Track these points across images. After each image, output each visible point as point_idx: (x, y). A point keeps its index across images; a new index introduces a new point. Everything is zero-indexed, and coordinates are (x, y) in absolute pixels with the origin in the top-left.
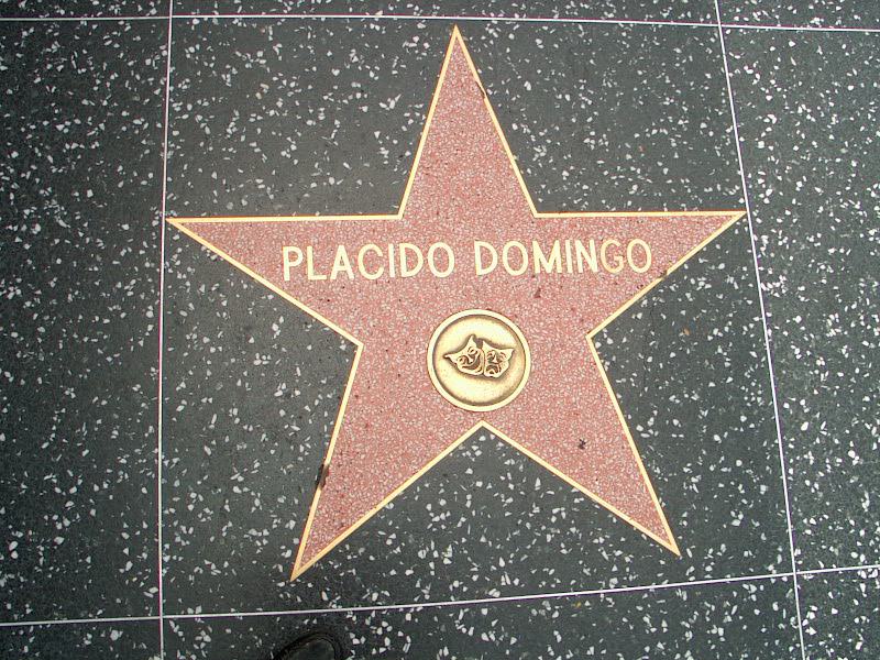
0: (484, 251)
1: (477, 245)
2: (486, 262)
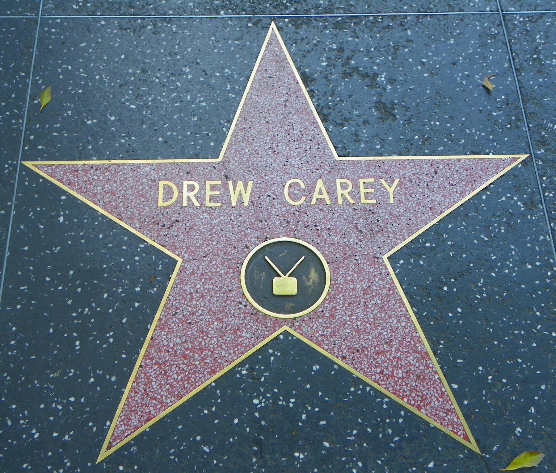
0: (166, 187)
1: (162, 183)
2: (168, 192)
